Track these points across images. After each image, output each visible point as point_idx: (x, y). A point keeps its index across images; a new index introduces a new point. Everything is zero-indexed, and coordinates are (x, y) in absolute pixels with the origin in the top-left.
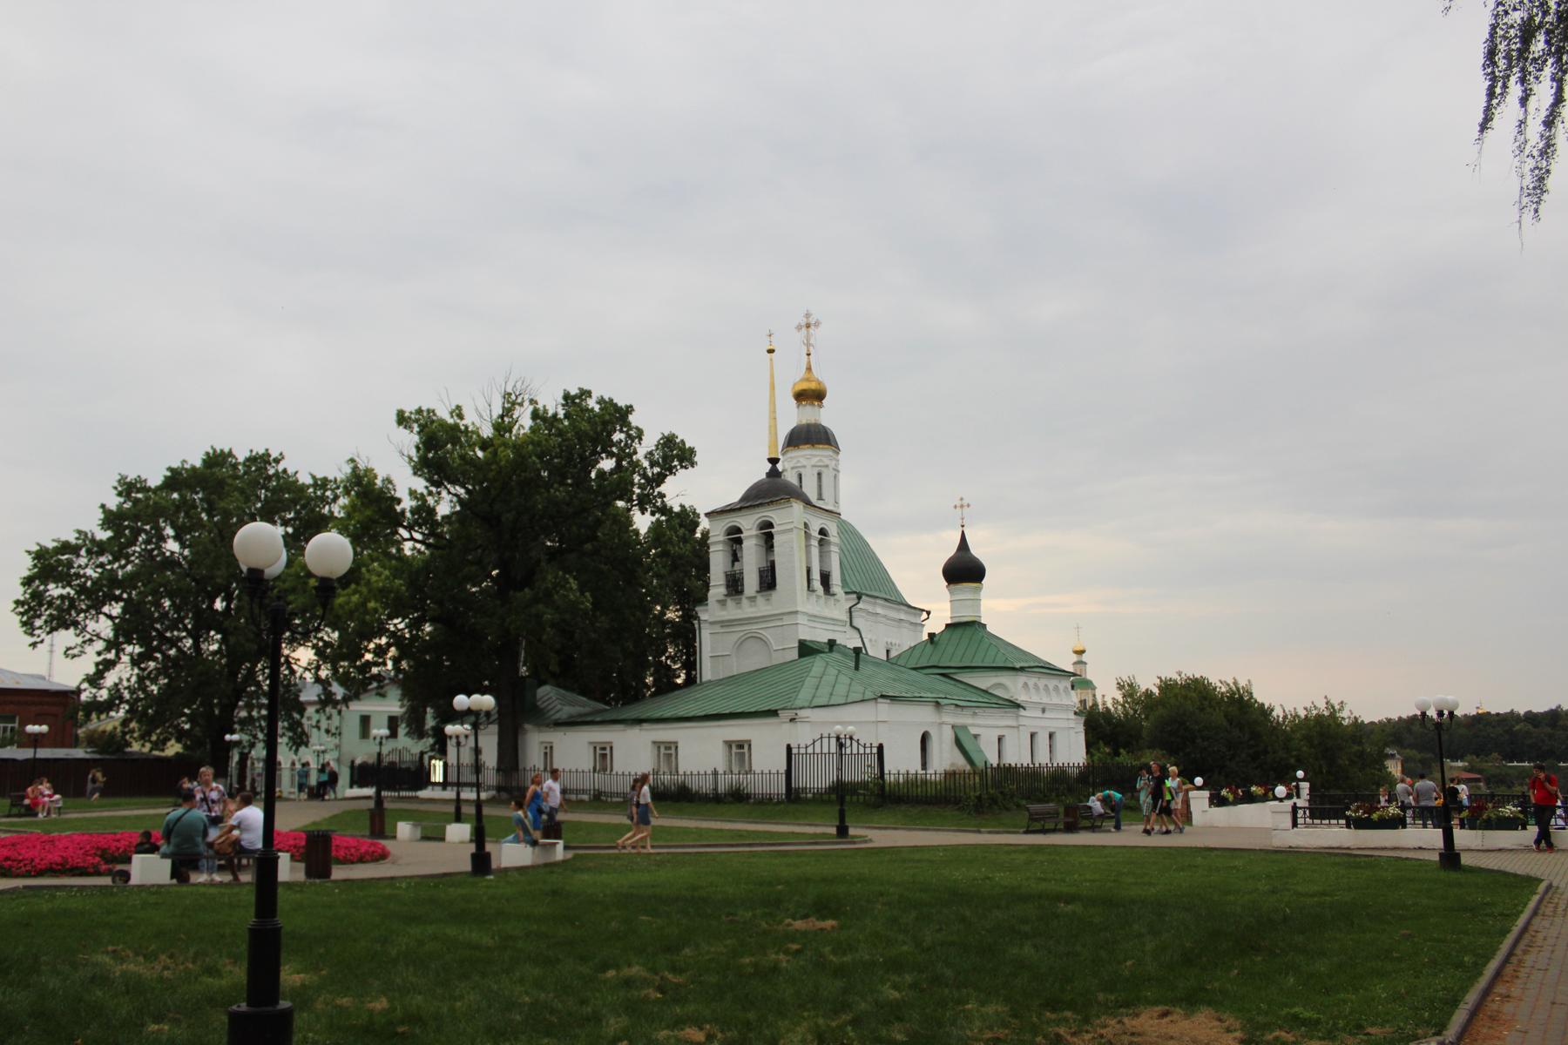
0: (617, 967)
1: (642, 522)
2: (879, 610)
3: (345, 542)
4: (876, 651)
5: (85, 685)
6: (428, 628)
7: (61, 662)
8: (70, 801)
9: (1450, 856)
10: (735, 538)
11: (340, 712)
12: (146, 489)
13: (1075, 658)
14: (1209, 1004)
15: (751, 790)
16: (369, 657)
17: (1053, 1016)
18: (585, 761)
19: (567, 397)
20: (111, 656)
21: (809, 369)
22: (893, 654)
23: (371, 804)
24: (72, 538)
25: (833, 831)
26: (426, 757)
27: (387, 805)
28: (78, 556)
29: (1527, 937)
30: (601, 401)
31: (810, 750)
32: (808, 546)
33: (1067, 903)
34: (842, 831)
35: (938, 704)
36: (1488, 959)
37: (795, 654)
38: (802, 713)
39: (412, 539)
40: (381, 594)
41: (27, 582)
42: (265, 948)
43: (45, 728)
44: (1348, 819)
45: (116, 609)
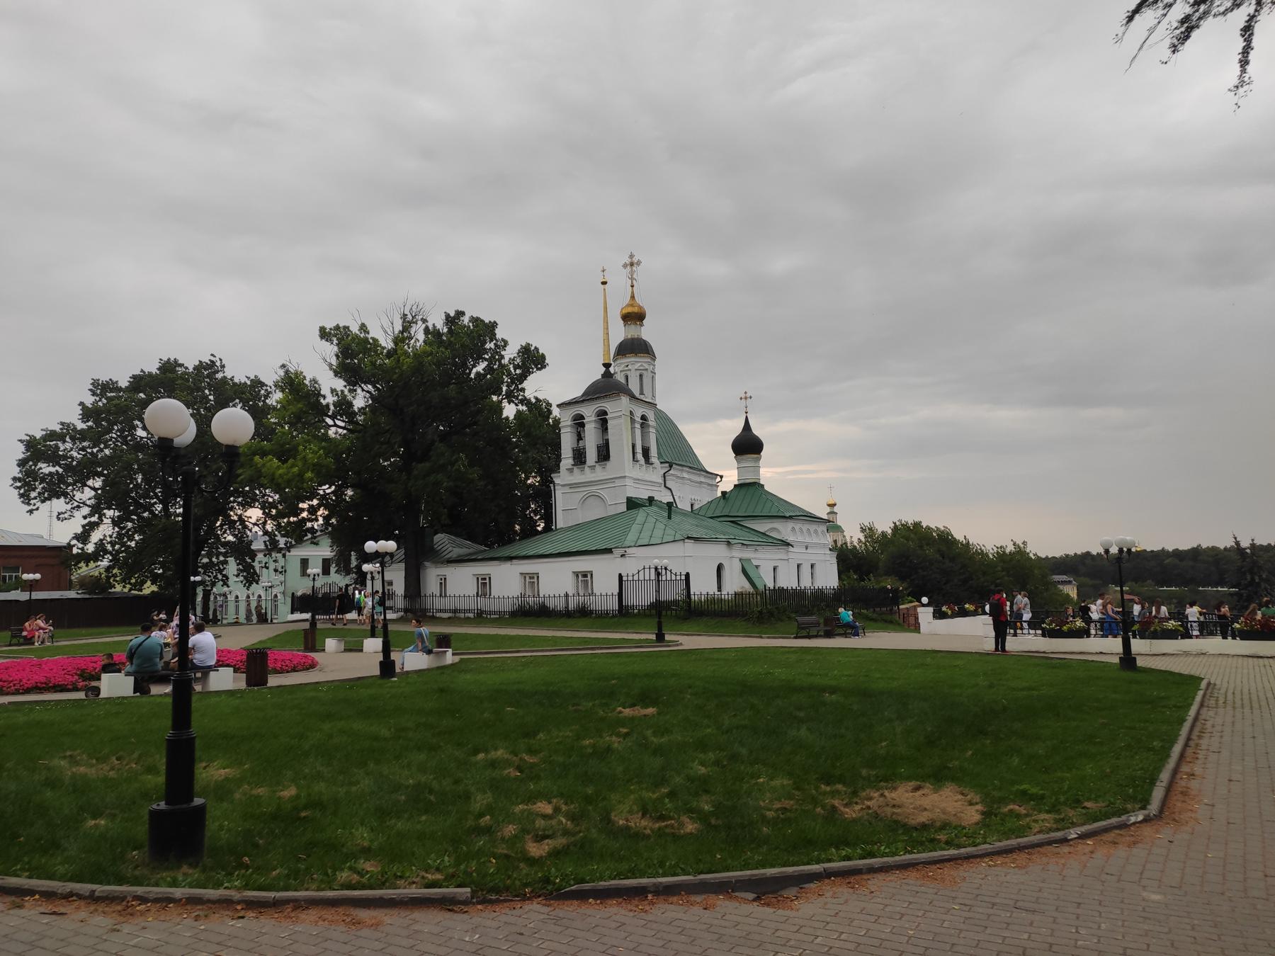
0: (486, 751)
1: (509, 411)
2: (685, 475)
4: (684, 505)
7: (53, 524)
8: (60, 632)
9: (1128, 659)
10: (579, 422)
11: (284, 556)
13: (828, 509)
14: (954, 779)
15: (593, 607)
16: (305, 514)
17: (828, 789)
18: (470, 588)
19: (448, 316)
20: (95, 519)
21: (633, 297)
22: (696, 507)
23: (307, 626)
24: (57, 428)
25: (653, 637)
27: (319, 626)
28: (64, 442)
29: (1198, 724)
31: (636, 578)
32: (633, 428)
33: (832, 693)
34: (660, 637)
36: (1173, 742)
37: (624, 508)
39: (335, 425)
40: (317, 468)
41: (22, 463)
42: (181, 755)
43: (38, 576)
44: (1043, 629)
45: (98, 483)
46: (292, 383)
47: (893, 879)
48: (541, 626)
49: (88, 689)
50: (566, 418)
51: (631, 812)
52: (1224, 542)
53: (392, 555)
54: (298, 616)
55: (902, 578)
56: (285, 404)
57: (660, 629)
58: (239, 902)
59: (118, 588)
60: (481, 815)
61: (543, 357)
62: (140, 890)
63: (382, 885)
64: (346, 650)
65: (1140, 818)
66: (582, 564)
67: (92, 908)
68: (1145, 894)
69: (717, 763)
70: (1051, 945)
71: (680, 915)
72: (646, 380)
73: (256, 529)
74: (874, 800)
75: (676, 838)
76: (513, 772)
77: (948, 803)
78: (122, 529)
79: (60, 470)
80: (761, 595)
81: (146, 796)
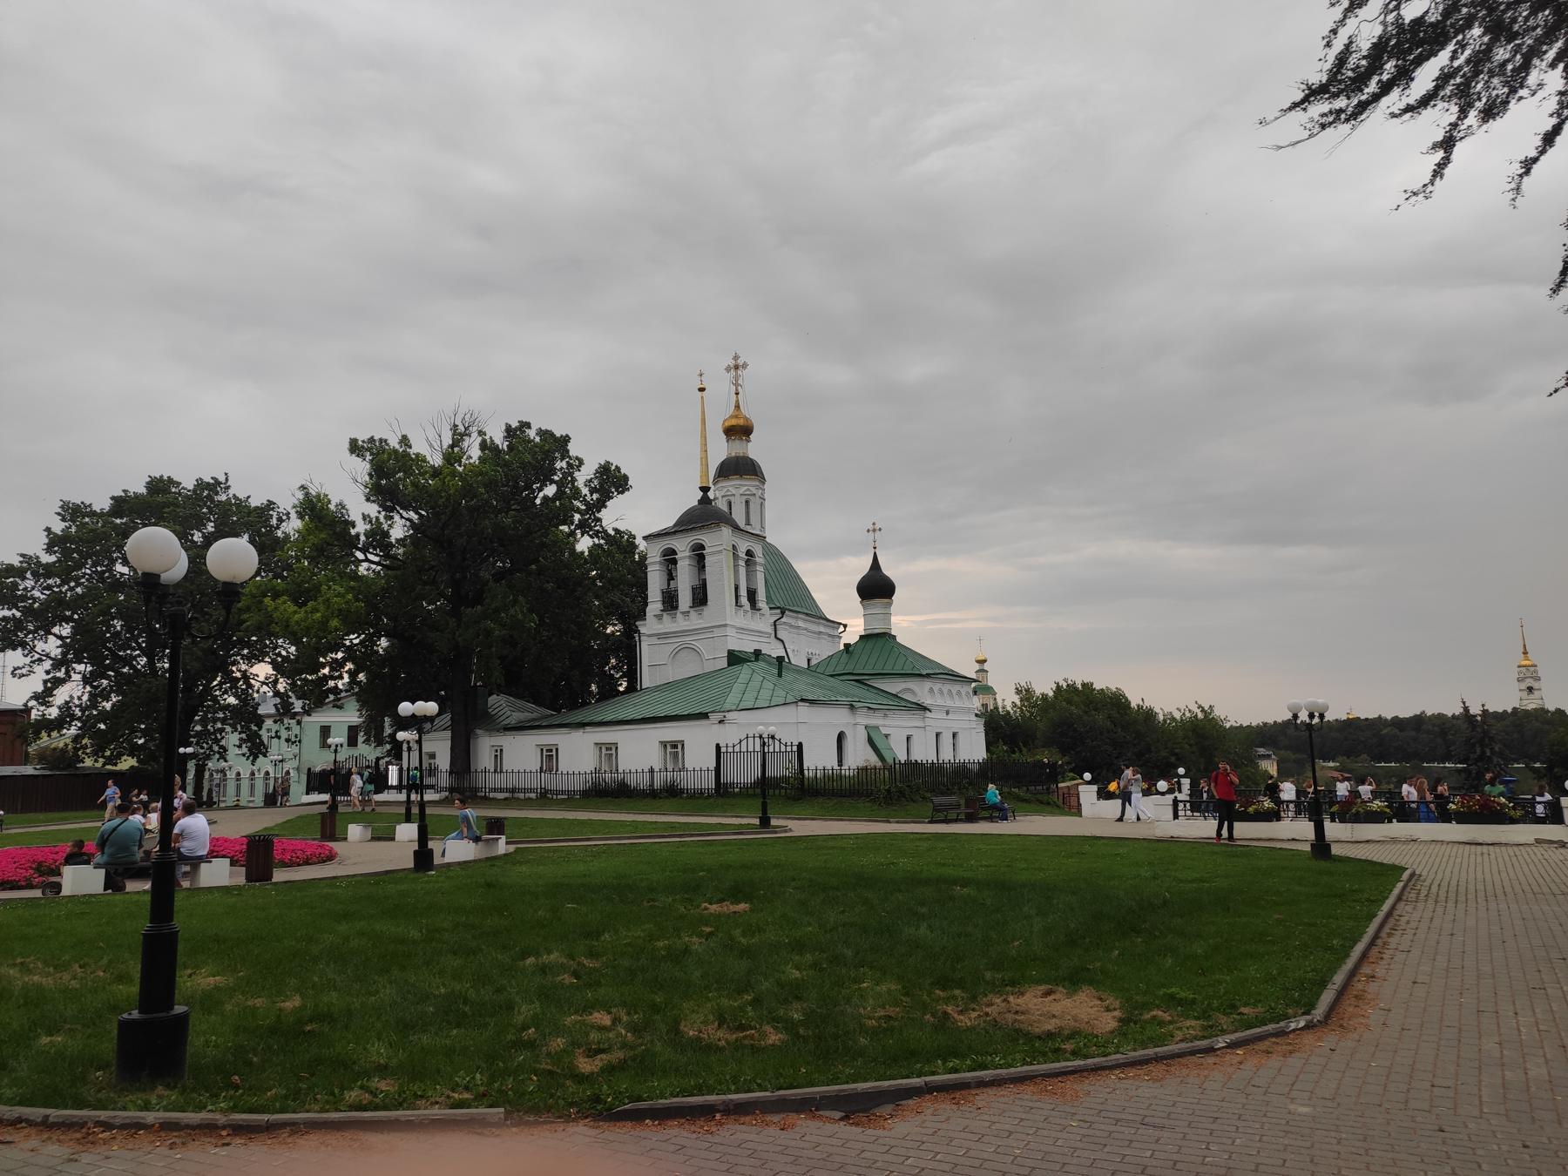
0: (537, 954)
1: (584, 544)
2: (801, 624)
3: (253, 553)
4: (799, 661)
5: (32, 703)
6: (384, 642)
10: (670, 558)
11: (299, 723)
12: (93, 514)
13: (977, 667)
14: (1091, 984)
15: (684, 785)
16: (326, 671)
18: (533, 762)
19: (509, 429)
20: (61, 674)
21: (737, 407)
22: (813, 662)
24: (16, 561)
25: (757, 821)
26: (382, 762)
27: (341, 809)
28: (24, 578)
30: (541, 432)
32: (736, 566)
34: (765, 822)
35: (852, 707)
36: (1355, 942)
38: (729, 716)
39: (367, 560)
42: (160, 954)
45: (66, 630)
46: (314, 508)
47: (1004, 1096)
48: (620, 809)
49: (44, 887)
50: (654, 554)
51: (705, 1022)
52: (1452, 709)
53: (430, 719)
54: (316, 797)
55: (1064, 751)
56: (304, 534)
57: (764, 811)
58: (224, 1127)
59: (88, 762)
60: (525, 1028)
61: (626, 478)
62: (103, 1115)
63: (399, 1106)
64: (373, 839)
65: (1302, 1024)
66: (671, 732)
67: (46, 1136)
68: (1292, 1107)
69: (815, 965)
70: (1175, 1162)
71: (751, 1137)
72: (754, 507)
73: (265, 688)
74: (996, 1006)
75: (755, 1050)
76: (568, 979)
77: (1086, 1009)
78: (95, 688)
79: (18, 614)
80: (890, 770)
81: (115, 1009)
